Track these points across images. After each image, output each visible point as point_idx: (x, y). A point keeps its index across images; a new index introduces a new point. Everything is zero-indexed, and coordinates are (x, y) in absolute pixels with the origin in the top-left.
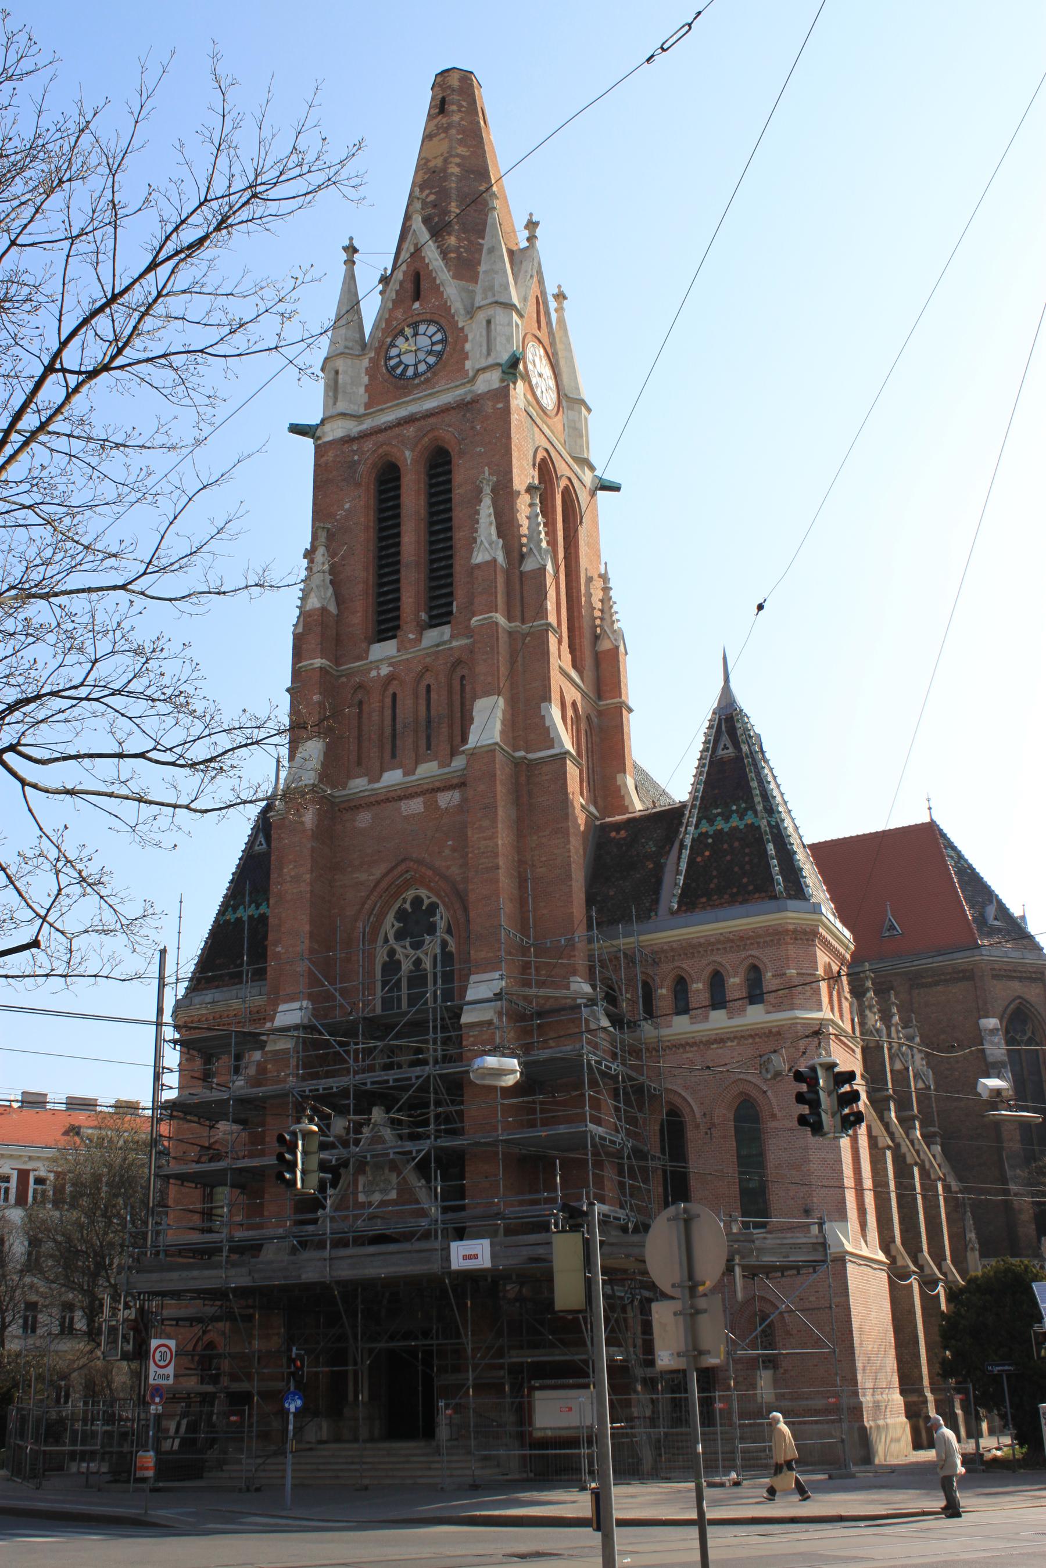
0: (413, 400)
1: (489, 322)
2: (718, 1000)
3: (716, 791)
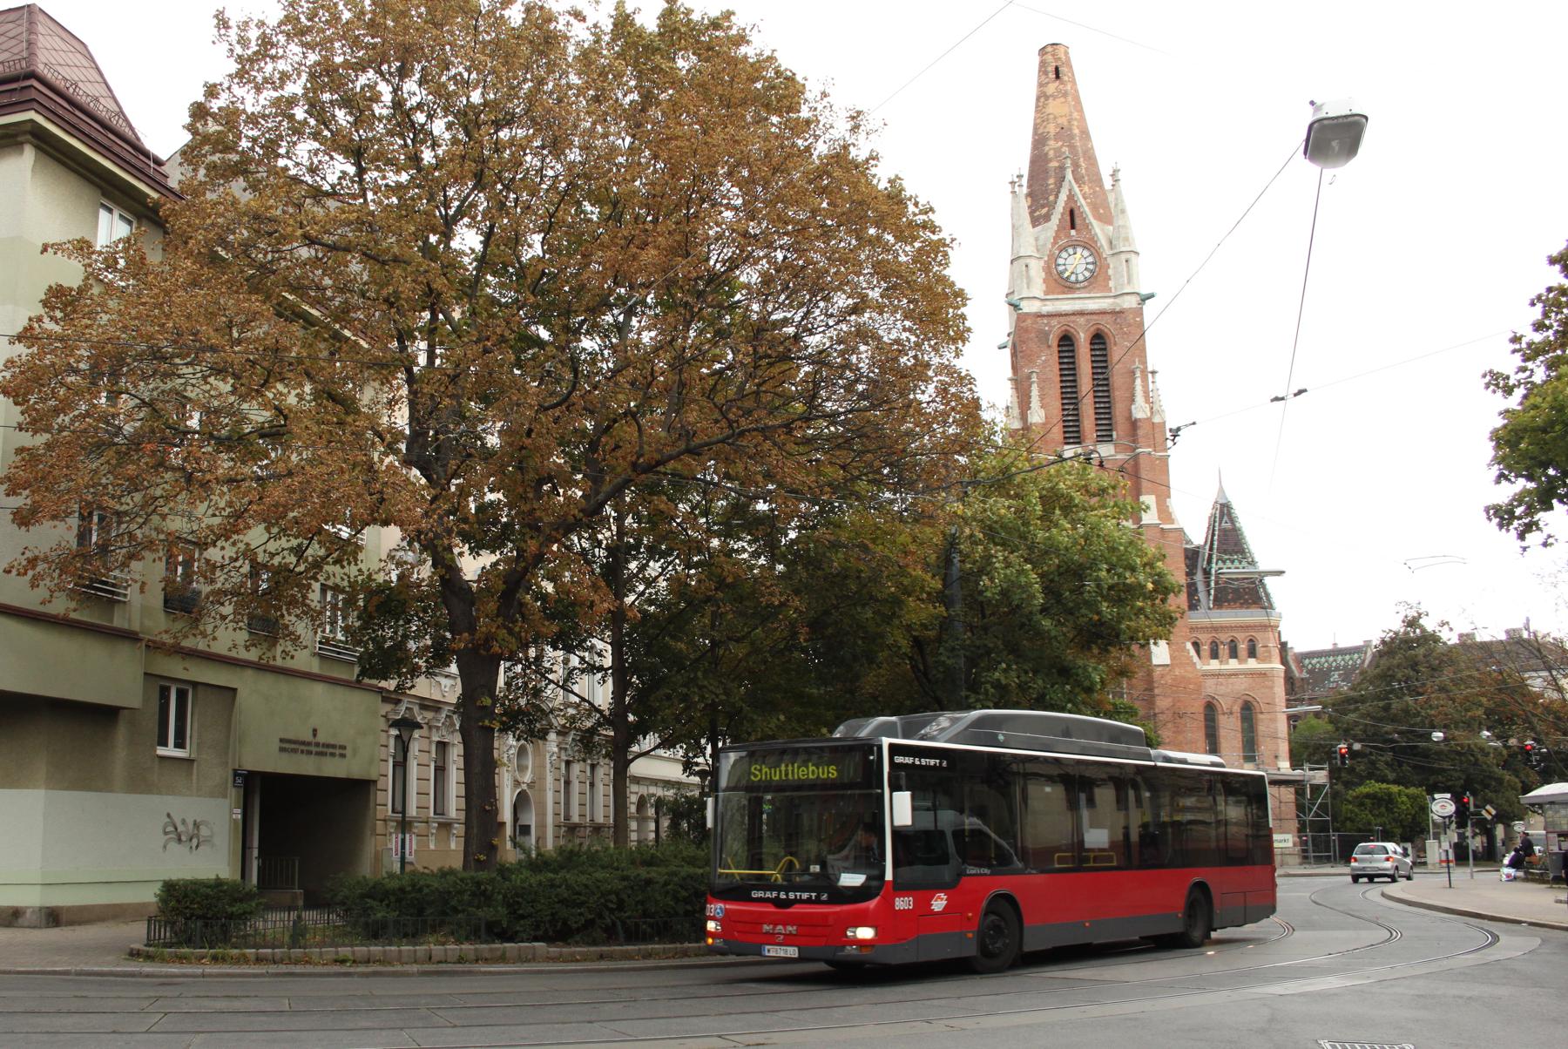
2: (1234, 653)
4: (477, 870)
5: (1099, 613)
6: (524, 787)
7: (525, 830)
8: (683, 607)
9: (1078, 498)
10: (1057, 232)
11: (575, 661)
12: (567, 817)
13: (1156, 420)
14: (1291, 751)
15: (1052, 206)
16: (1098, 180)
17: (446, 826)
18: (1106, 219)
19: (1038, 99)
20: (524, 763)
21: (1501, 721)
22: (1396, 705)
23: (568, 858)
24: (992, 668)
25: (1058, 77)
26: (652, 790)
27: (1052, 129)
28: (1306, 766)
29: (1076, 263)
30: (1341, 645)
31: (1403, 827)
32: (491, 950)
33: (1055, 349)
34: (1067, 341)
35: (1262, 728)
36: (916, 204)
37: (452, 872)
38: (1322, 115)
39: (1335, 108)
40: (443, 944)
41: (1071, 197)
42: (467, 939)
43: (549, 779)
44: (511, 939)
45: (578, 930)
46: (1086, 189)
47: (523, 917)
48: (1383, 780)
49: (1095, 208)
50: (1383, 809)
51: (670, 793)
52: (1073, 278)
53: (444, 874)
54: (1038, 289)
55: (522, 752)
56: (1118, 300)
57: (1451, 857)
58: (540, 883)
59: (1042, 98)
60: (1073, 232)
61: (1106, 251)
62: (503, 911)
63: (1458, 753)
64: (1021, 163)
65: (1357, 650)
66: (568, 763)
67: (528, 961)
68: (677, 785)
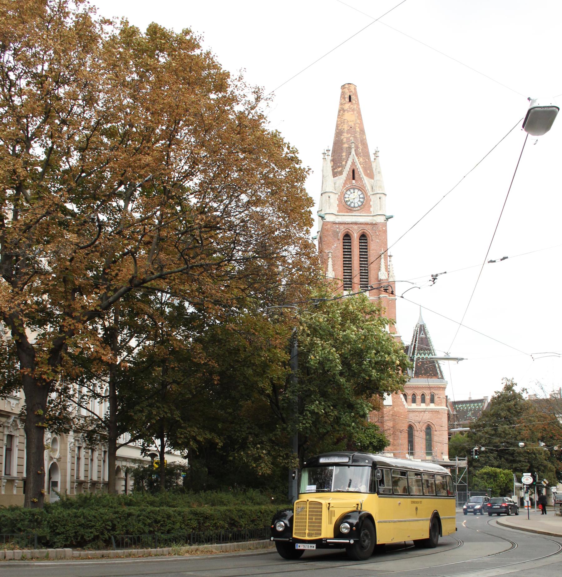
2: (423, 401)
4: (32, 507)
5: (370, 376)
6: (55, 460)
7: (55, 484)
8: (148, 361)
9: (360, 315)
10: (345, 181)
11: (85, 390)
12: (78, 478)
13: (391, 280)
14: (449, 452)
15: (343, 167)
16: (367, 155)
17: (11, 481)
18: (371, 176)
19: (339, 111)
20: (55, 447)
21: (549, 439)
22: (500, 429)
23: (84, 502)
24: (312, 402)
25: (350, 101)
26: (124, 463)
27: (346, 127)
28: (457, 458)
29: (354, 197)
30: (474, 398)
31: (501, 489)
32: (40, 552)
33: (341, 241)
34: (347, 237)
35: (435, 438)
36: (288, 148)
37: (17, 508)
38: (535, 105)
39: (543, 102)
40: (13, 549)
41: (353, 163)
42: (26, 546)
43: (69, 456)
44: (51, 546)
45: (90, 541)
46: (361, 160)
47: (59, 534)
48: (492, 466)
49: (365, 170)
50: (492, 480)
51: (136, 466)
52: (352, 205)
53: (13, 509)
54: (335, 210)
55: (54, 441)
56: (375, 218)
57: (530, 505)
58: (69, 515)
59: (342, 111)
60: (354, 181)
61: (370, 193)
62: (47, 530)
63: (528, 453)
64: (330, 145)
65: (481, 401)
66: (79, 448)
67: (61, 559)
68: (140, 461)
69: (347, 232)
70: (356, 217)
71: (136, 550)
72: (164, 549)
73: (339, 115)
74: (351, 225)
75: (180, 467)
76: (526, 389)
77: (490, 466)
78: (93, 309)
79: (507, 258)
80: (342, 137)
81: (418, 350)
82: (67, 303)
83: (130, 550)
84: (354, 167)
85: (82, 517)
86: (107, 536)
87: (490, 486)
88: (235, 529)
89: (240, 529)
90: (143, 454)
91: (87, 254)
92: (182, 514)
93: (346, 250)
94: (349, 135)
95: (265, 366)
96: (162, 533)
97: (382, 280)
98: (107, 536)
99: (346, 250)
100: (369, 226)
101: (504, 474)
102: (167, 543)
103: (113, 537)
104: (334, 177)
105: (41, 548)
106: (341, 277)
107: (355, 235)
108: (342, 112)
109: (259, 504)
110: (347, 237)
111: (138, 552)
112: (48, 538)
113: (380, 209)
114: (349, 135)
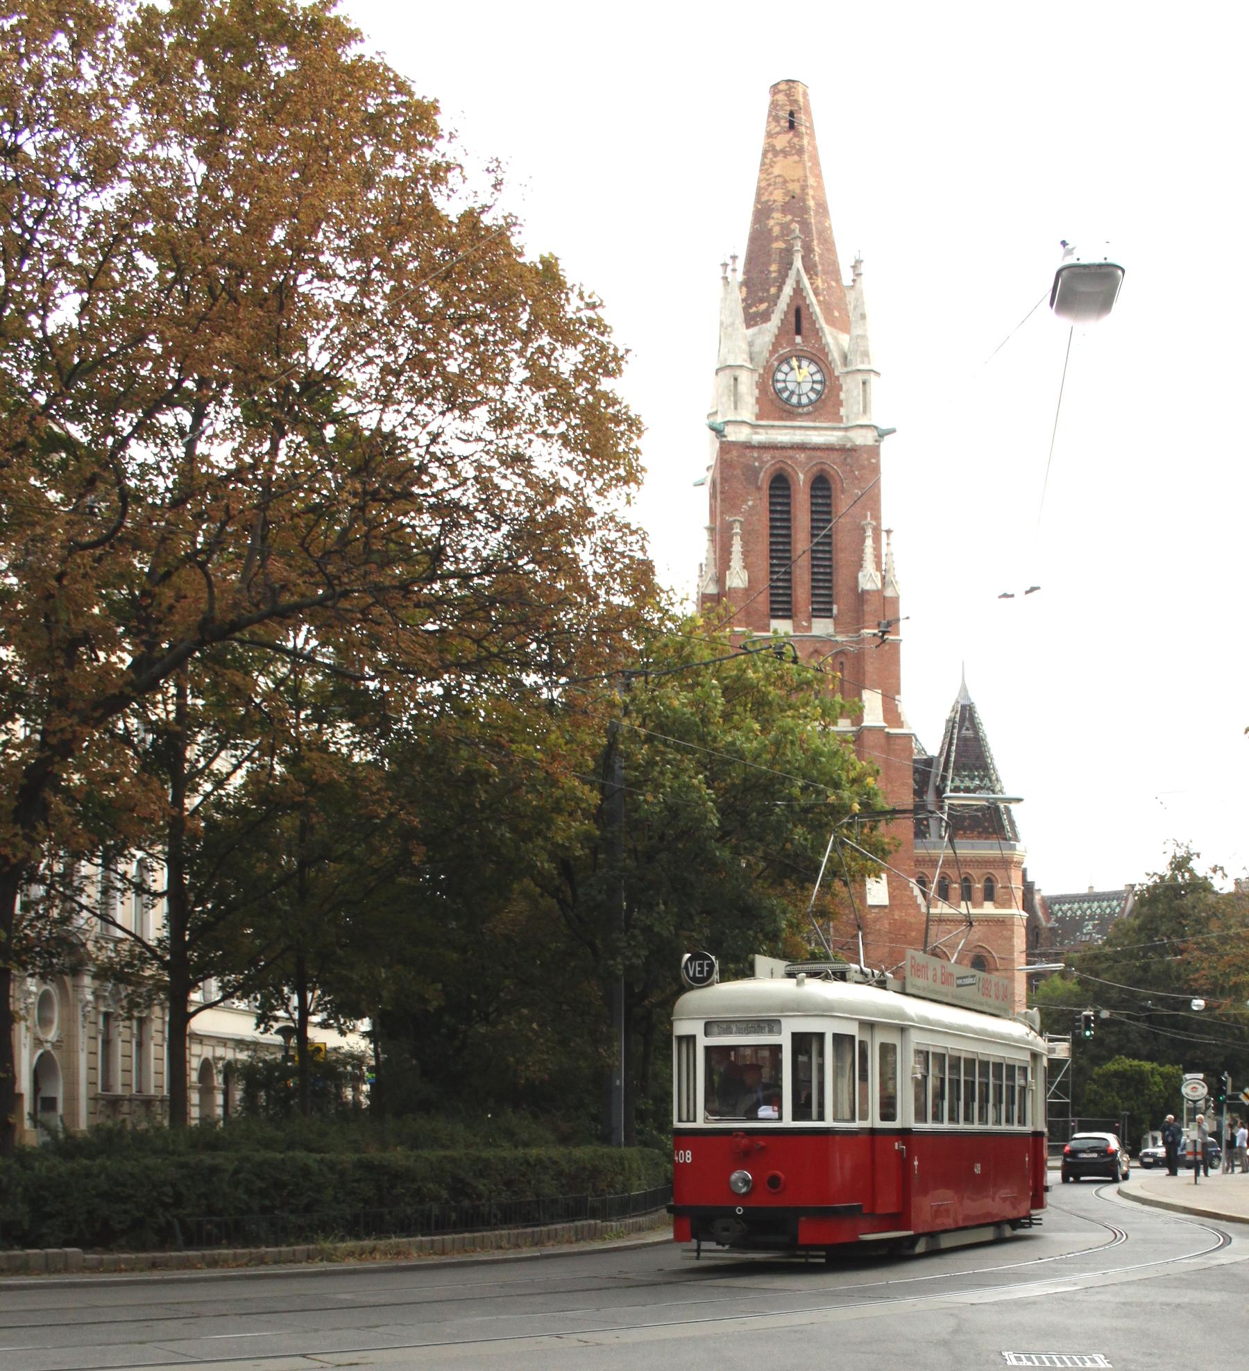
0: (801, 428)
1: (864, 383)
2: (967, 895)
3: (222, 282)
6: (48, 1047)
10: (777, 337)
13: (889, 593)
15: (775, 300)
19: (764, 155)
27: (778, 196)
29: (800, 378)
30: (1100, 888)
33: (766, 492)
34: (780, 484)
39: (1089, 255)
41: (798, 291)
48: (1135, 1055)
49: (827, 308)
50: (1131, 1091)
51: (243, 1056)
54: (748, 412)
56: (852, 434)
60: (798, 339)
61: (839, 370)
65: (1116, 896)
69: (781, 469)
70: (803, 432)
71: (230, 1252)
72: (296, 1248)
73: (763, 164)
74: (791, 452)
75: (356, 1059)
76: (1222, 868)
77: (1128, 1056)
78: (116, 691)
79: (1038, 588)
80: (771, 222)
81: (956, 769)
82: (56, 676)
83: (216, 1252)
84: (800, 302)
85: (103, 1176)
86: (162, 1220)
87: (1126, 1105)
88: (466, 1203)
89: (477, 1203)
90: (262, 1026)
91: (99, 560)
92: (340, 1167)
93: (778, 516)
94: (789, 217)
95: (543, 818)
96: (292, 1212)
97: (868, 592)
98: (162, 1220)
99: (778, 516)
100: (835, 455)
101: (1161, 1074)
102: (302, 1234)
103: (176, 1223)
104: (748, 326)
105: (11, 1248)
106: (764, 585)
107: (801, 476)
108: (770, 155)
109: (526, 1145)
110: (780, 484)
111: (235, 1255)
112: (26, 1226)
113: (865, 412)
114: (789, 217)
